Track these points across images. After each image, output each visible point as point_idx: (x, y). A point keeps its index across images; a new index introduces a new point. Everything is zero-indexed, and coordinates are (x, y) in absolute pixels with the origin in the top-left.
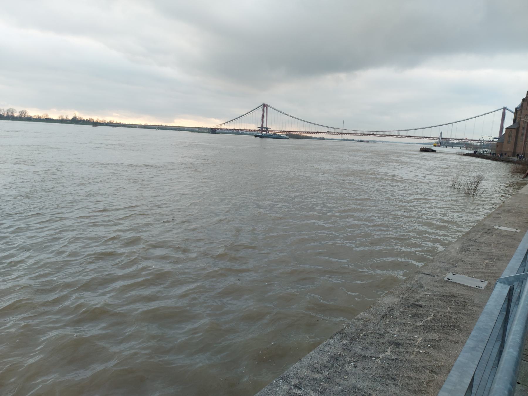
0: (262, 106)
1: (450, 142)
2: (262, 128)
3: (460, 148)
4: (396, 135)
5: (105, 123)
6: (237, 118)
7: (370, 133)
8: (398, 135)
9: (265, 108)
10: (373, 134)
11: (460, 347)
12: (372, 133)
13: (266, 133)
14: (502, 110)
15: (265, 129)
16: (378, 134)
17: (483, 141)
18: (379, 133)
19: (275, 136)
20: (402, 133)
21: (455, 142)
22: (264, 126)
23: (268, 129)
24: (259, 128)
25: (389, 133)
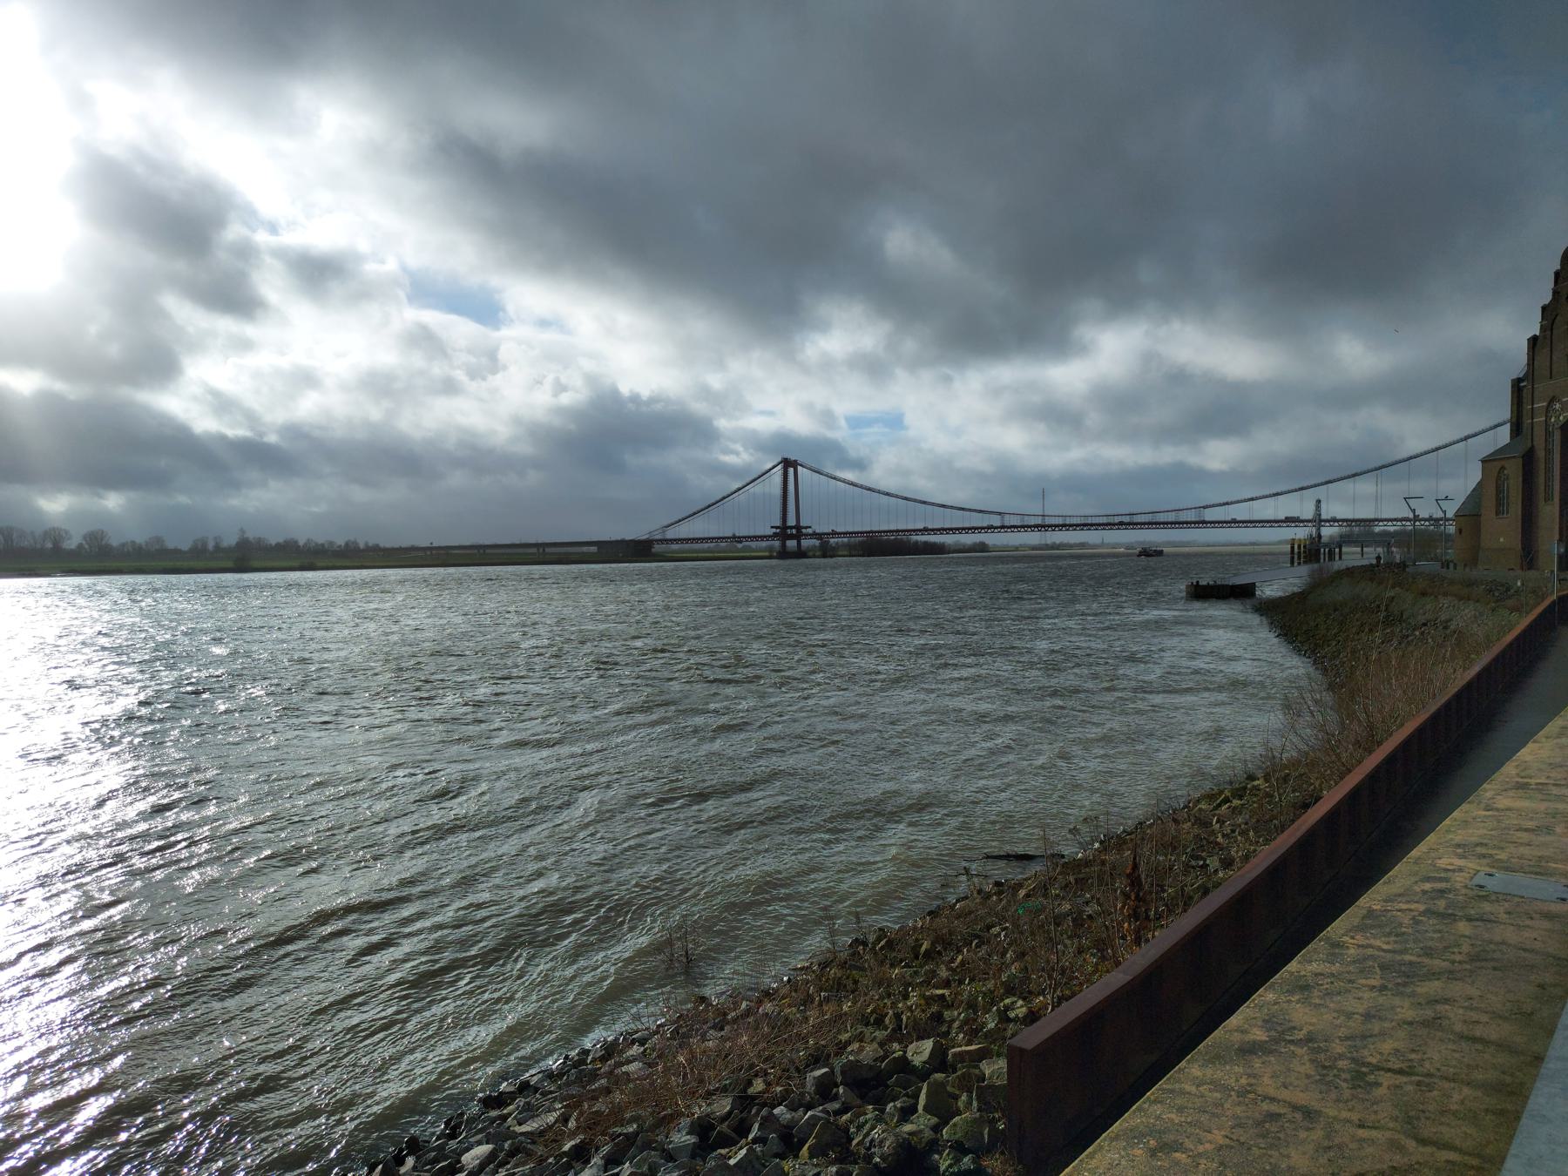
0: (780, 467)
1: (1377, 529)
2: (784, 527)
3: (1359, 549)
4: (1193, 519)
5: (1047, 545)
6: (695, 514)
7: (1111, 520)
8: (1197, 519)
9: (791, 470)
10: (1121, 523)
11: (1090, 927)
12: (1117, 520)
13: (799, 544)
14: (1509, 424)
15: (794, 531)
16: (1158, 520)
17: (1441, 519)
18: (1161, 518)
19: (827, 548)
20: (1210, 515)
21: (1392, 529)
22: (791, 522)
23: (804, 531)
24: (777, 528)
25: (1171, 517)
